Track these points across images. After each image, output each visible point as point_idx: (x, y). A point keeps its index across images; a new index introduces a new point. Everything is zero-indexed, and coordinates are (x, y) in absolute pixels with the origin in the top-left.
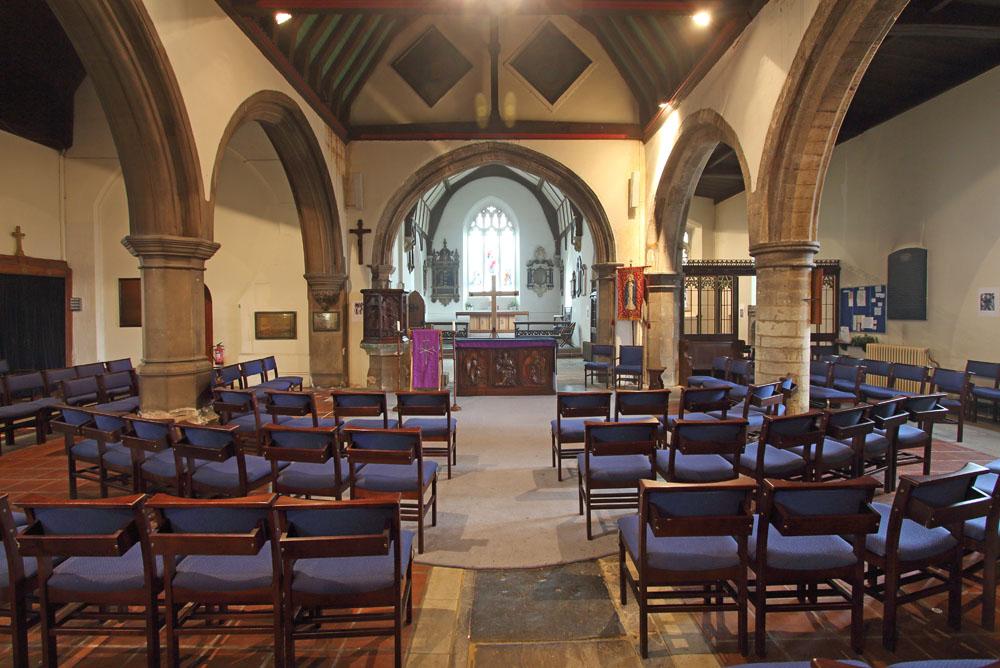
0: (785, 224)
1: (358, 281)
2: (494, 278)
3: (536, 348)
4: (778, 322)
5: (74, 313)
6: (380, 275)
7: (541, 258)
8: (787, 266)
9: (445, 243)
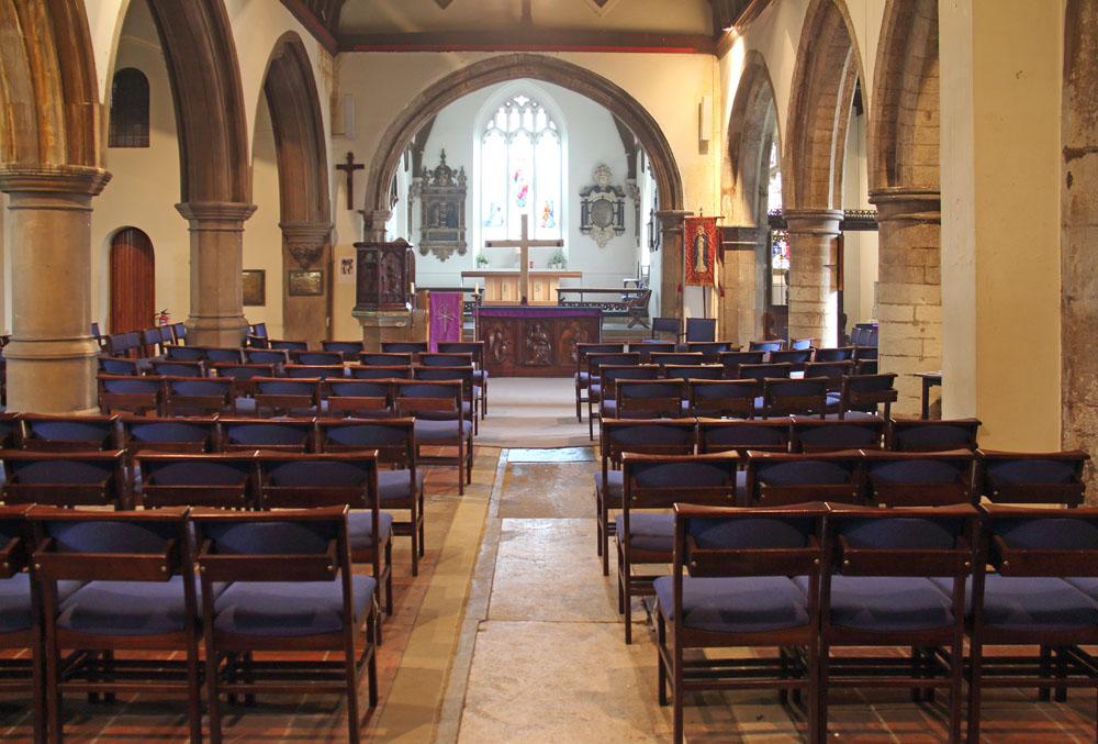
0: (805, 192)
1: (346, 233)
2: (524, 219)
3: (576, 318)
4: (802, 287)
6: (375, 223)
7: (603, 182)
8: (808, 233)
9: (443, 156)
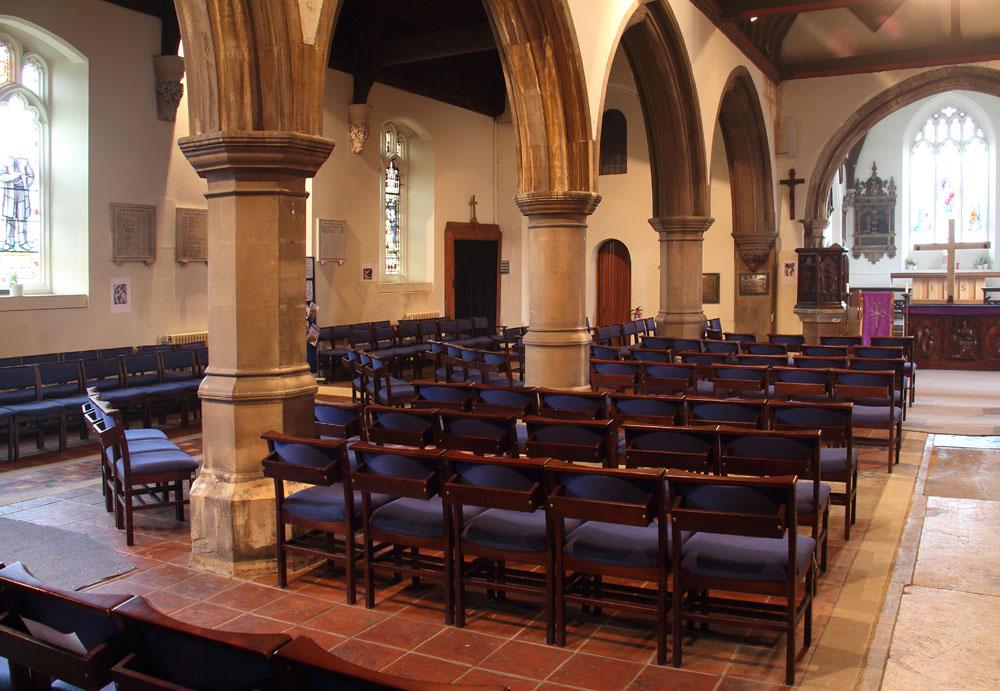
1: (789, 240)
2: (952, 223)
5: (503, 276)
6: (814, 231)
9: (874, 168)
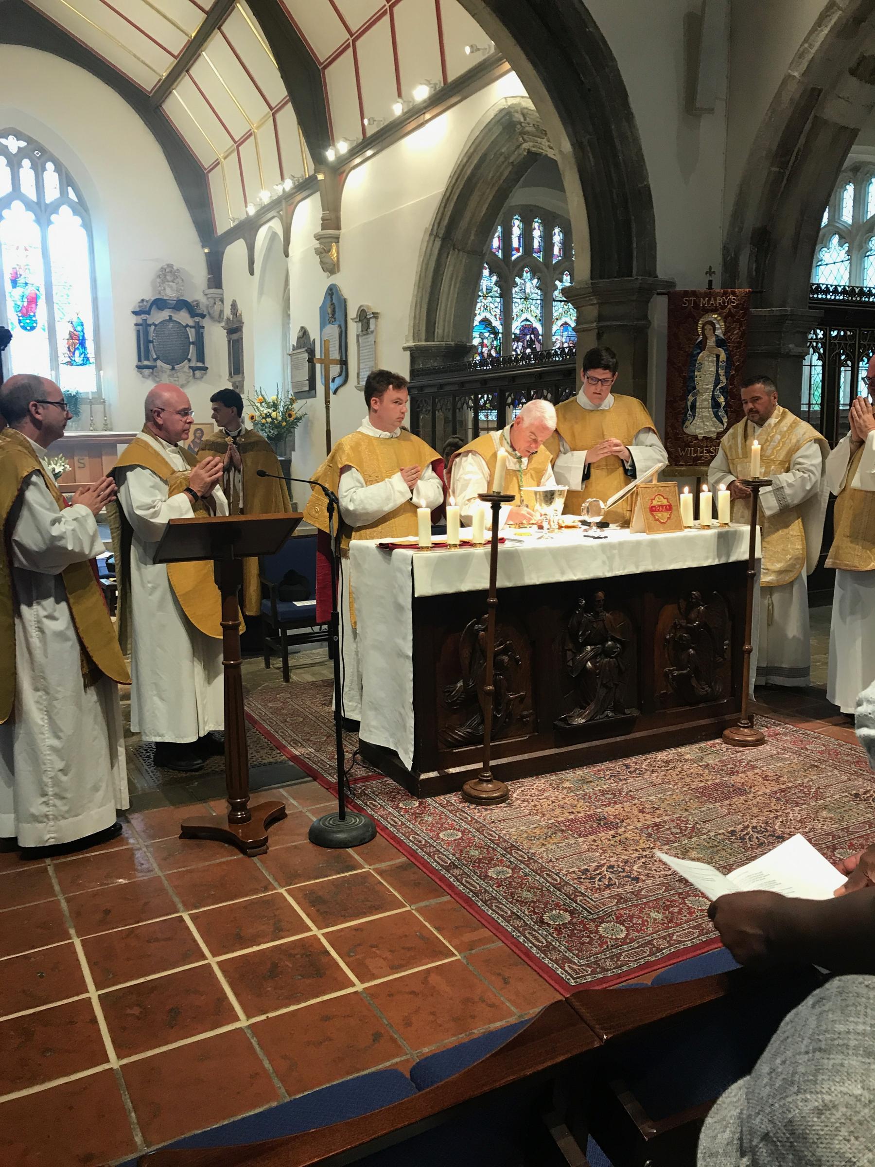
7: (170, 294)
